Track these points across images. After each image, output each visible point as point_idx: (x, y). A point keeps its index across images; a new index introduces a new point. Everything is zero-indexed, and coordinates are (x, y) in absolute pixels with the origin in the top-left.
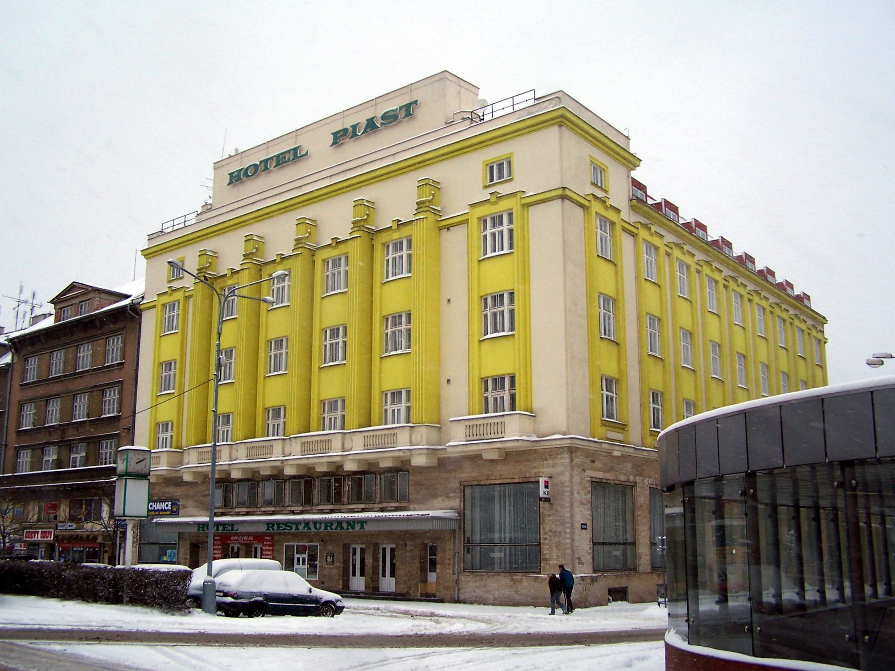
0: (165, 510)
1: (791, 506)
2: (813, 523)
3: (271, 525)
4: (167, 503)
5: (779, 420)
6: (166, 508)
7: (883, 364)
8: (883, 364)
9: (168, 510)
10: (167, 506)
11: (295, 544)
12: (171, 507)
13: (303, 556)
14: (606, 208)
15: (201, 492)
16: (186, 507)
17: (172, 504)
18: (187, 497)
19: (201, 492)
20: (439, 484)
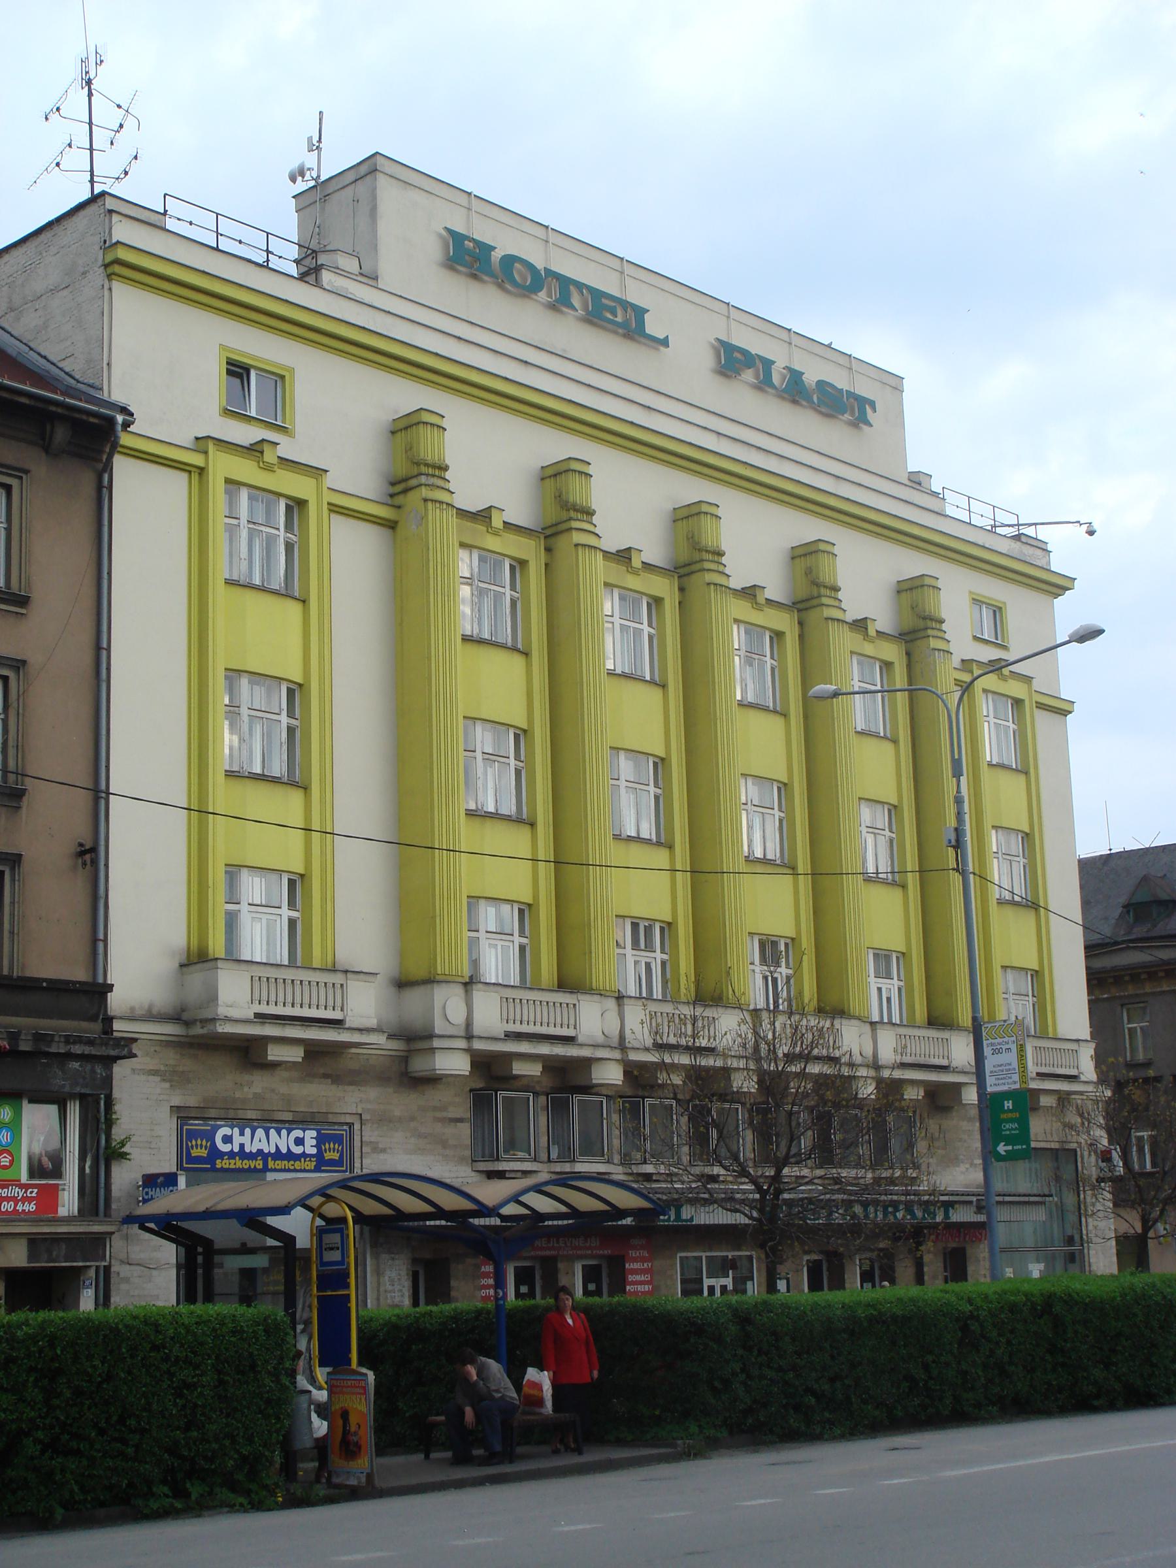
0: (290, 1156)
1: (112, 794)
2: (237, 1245)
3: (890, 1209)
4: (298, 1133)
5: (308, 210)
6: (298, 1150)
7: (931, 476)
8: (931, 476)
9: (304, 1155)
10: (299, 1142)
11: (704, 1255)
12: (318, 1146)
13: (723, 1281)
14: (757, 606)
15: (435, 1109)
16: (384, 1151)
17: (321, 1140)
18: (384, 1120)
19: (435, 1109)
20: (960, 1140)
